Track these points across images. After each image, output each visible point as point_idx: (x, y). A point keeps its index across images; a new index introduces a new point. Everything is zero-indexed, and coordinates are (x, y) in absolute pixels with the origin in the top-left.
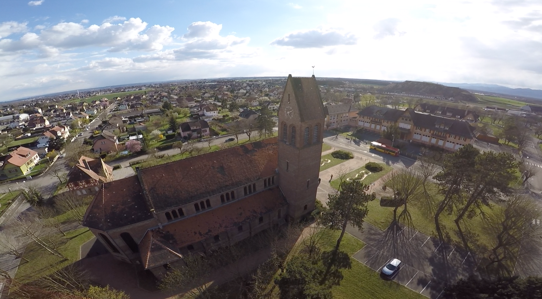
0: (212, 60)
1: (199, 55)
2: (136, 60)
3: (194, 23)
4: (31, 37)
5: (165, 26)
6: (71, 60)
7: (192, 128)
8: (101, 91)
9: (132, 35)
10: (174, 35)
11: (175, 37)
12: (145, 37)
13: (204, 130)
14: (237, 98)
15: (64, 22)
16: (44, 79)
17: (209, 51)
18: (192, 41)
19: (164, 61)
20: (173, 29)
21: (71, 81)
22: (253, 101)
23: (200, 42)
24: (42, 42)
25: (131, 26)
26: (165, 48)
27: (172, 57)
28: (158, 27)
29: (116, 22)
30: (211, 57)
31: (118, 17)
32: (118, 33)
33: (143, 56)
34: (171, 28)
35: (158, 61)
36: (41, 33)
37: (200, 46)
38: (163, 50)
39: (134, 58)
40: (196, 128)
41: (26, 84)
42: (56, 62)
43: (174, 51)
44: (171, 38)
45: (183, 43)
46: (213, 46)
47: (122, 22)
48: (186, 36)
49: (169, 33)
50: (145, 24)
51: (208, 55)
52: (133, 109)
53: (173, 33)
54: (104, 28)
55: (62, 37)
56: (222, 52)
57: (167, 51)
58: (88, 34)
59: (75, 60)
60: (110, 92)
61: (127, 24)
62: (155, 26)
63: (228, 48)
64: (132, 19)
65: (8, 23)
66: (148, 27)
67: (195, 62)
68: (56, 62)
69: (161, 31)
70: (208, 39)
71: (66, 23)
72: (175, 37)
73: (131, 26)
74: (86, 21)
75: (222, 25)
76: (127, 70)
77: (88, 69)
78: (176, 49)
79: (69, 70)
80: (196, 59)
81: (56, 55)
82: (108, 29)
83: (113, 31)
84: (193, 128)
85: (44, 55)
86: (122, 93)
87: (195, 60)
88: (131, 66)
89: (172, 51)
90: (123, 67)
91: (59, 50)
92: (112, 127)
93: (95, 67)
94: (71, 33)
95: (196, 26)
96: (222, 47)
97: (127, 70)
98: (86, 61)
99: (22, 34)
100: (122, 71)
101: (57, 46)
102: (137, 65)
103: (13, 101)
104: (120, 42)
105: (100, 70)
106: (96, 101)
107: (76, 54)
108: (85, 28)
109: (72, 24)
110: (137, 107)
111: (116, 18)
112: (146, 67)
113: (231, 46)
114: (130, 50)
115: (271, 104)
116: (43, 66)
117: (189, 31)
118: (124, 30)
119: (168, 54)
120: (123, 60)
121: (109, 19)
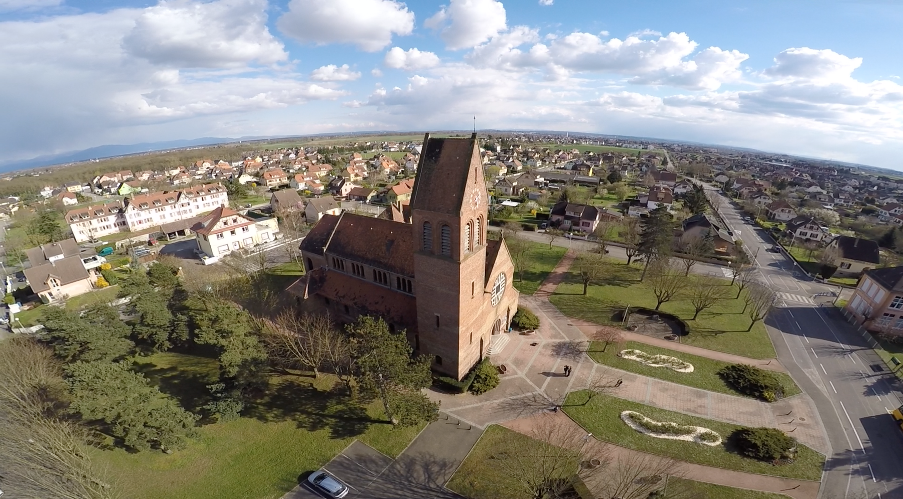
0: (820, 123)
1: (791, 110)
2: (668, 102)
3: (793, 49)
4: (540, 51)
5: (731, 51)
6: (579, 88)
7: (567, 213)
8: (636, 143)
9: (670, 60)
10: (747, 68)
11: (748, 71)
12: (691, 66)
13: (586, 223)
14: (760, 196)
15: (579, 32)
16: (544, 111)
17: (819, 105)
18: (785, 81)
19: (717, 110)
20: (746, 56)
21: (572, 118)
22: (780, 210)
23: (801, 85)
24: (551, 58)
25: (672, 45)
26: (724, 87)
27: (735, 105)
28: (717, 50)
29: (648, 38)
30: (821, 116)
31: (651, 31)
32: (648, 55)
33: (681, 97)
34: (742, 55)
35: (705, 108)
36: (551, 45)
37: (798, 94)
38: (720, 90)
39: (666, 97)
40: (573, 215)
41: (524, 113)
42: (561, 89)
43: (739, 94)
44: (741, 72)
45: (761, 83)
46: (831, 95)
47: (657, 39)
48: (769, 72)
49: (737, 63)
50: (694, 44)
51: (814, 111)
52: (575, 171)
53: (743, 65)
54: (629, 45)
55: (575, 54)
56: (850, 110)
57: (726, 94)
58: (607, 52)
59: (584, 89)
60: (601, 143)
61: (664, 43)
62: (712, 48)
63: (871, 105)
64: (673, 35)
65: (520, 27)
66: (697, 50)
67: (781, 120)
68: (561, 89)
69: (721, 59)
70: (820, 81)
71: (581, 34)
72: (748, 71)
73: (672, 45)
74: (605, 33)
75: (861, 59)
76: (650, 114)
77: (597, 104)
78: (745, 92)
79: (573, 103)
80: (783, 115)
81: (564, 78)
82: (634, 48)
83: (641, 52)
84: (570, 213)
85: (550, 77)
86: (617, 148)
87: (782, 117)
88: (659, 110)
89: (736, 94)
90: (645, 109)
91: (569, 72)
92: (505, 184)
93: (606, 103)
94: (585, 49)
95: (796, 56)
96: (855, 102)
97: (650, 114)
98: (597, 93)
99: (531, 45)
100: (643, 116)
101: (569, 65)
102: (669, 109)
103: (504, 131)
104: (649, 69)
105: (612, 109)
106: (590, 152)
107: (587, 80)
108: (603, 43)
109: (587, 35)
110: (580, 170)
111: (647, 32)
112: (682, 114)
113: (879, 101)
114: (663, 84)
115: (808, 226)
116: (546, 92)
117: (777, 63)
118: (659, 51)
119: (727, 98)
120: (649, 98)
121: (637, 33)
